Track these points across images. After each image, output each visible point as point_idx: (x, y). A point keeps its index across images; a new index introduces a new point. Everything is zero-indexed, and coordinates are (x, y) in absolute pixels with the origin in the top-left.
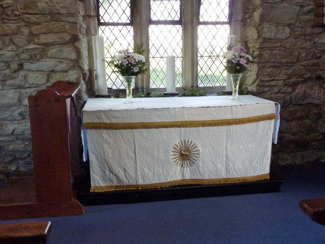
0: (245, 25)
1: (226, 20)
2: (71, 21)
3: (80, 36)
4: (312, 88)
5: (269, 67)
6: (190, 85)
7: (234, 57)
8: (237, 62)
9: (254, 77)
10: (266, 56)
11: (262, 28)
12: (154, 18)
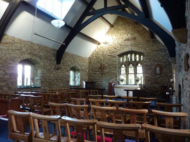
1: (133, 73)
4: (156, 85)
12: (129, 73)
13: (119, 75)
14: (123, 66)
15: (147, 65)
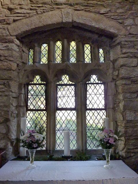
0: (114, 111)
2: (5, 110)
3: (11, 119)
5: (133, 139)
6: (81, 149)
7: (105, 137)
8: (107, 141)
9: (123, 146)
10: (130, 132)
11: (126, 114)
13: (18, 115)
14: (37, 78)
15: (128, 78)
